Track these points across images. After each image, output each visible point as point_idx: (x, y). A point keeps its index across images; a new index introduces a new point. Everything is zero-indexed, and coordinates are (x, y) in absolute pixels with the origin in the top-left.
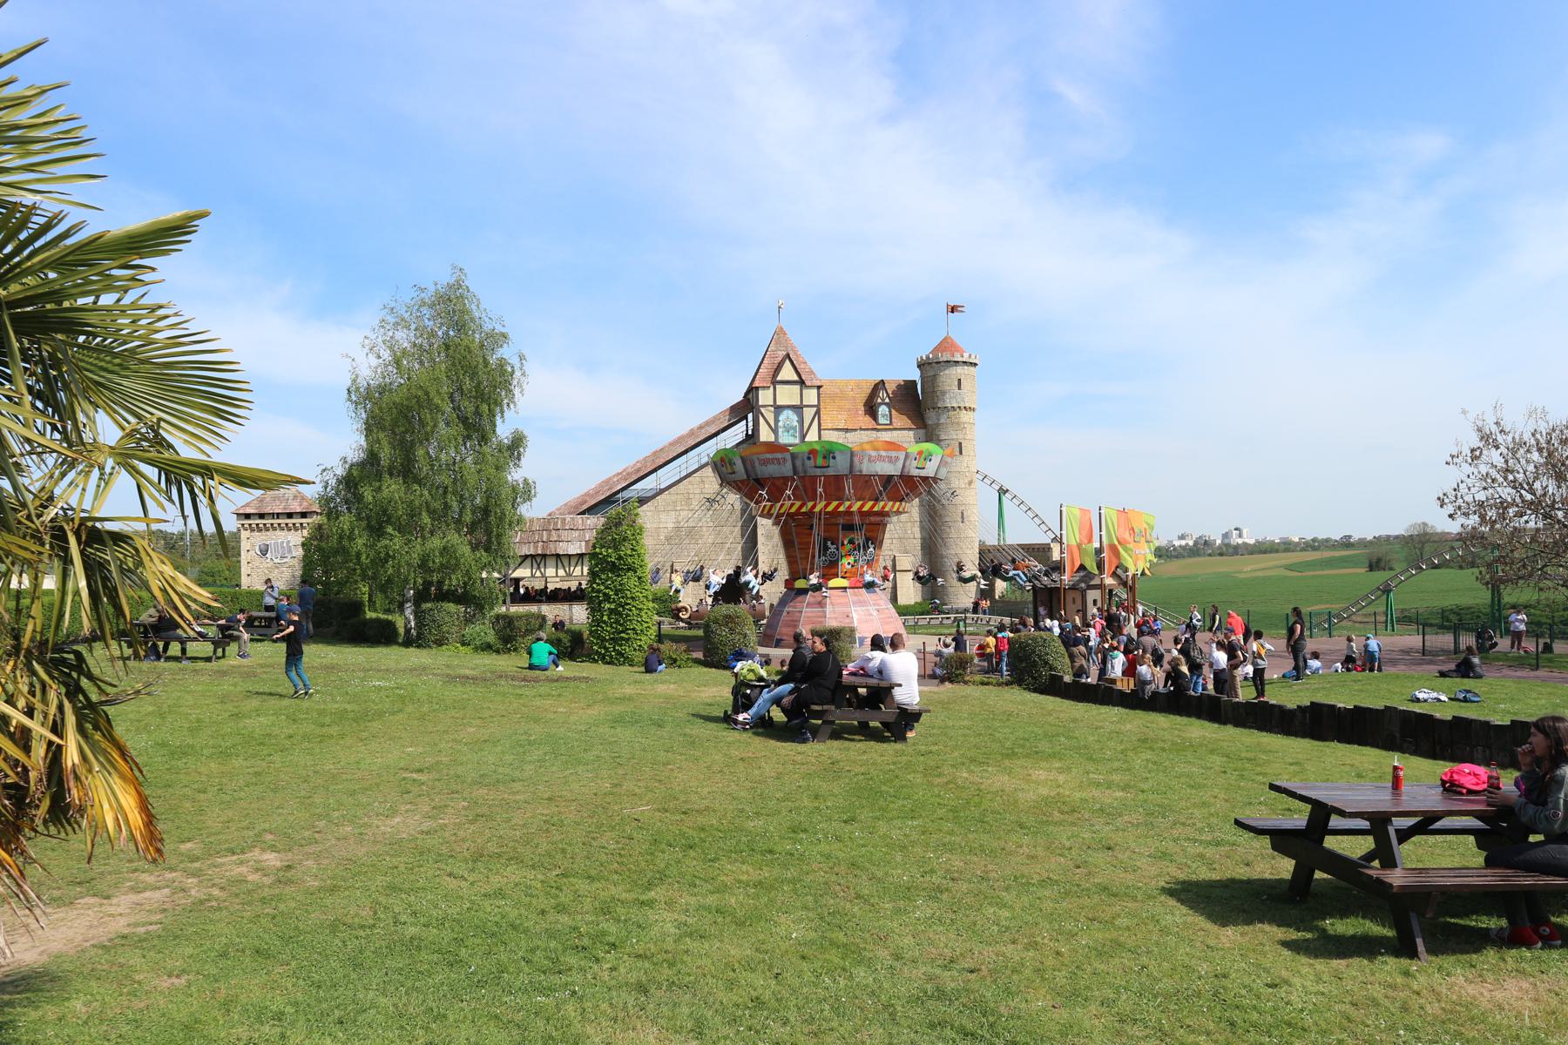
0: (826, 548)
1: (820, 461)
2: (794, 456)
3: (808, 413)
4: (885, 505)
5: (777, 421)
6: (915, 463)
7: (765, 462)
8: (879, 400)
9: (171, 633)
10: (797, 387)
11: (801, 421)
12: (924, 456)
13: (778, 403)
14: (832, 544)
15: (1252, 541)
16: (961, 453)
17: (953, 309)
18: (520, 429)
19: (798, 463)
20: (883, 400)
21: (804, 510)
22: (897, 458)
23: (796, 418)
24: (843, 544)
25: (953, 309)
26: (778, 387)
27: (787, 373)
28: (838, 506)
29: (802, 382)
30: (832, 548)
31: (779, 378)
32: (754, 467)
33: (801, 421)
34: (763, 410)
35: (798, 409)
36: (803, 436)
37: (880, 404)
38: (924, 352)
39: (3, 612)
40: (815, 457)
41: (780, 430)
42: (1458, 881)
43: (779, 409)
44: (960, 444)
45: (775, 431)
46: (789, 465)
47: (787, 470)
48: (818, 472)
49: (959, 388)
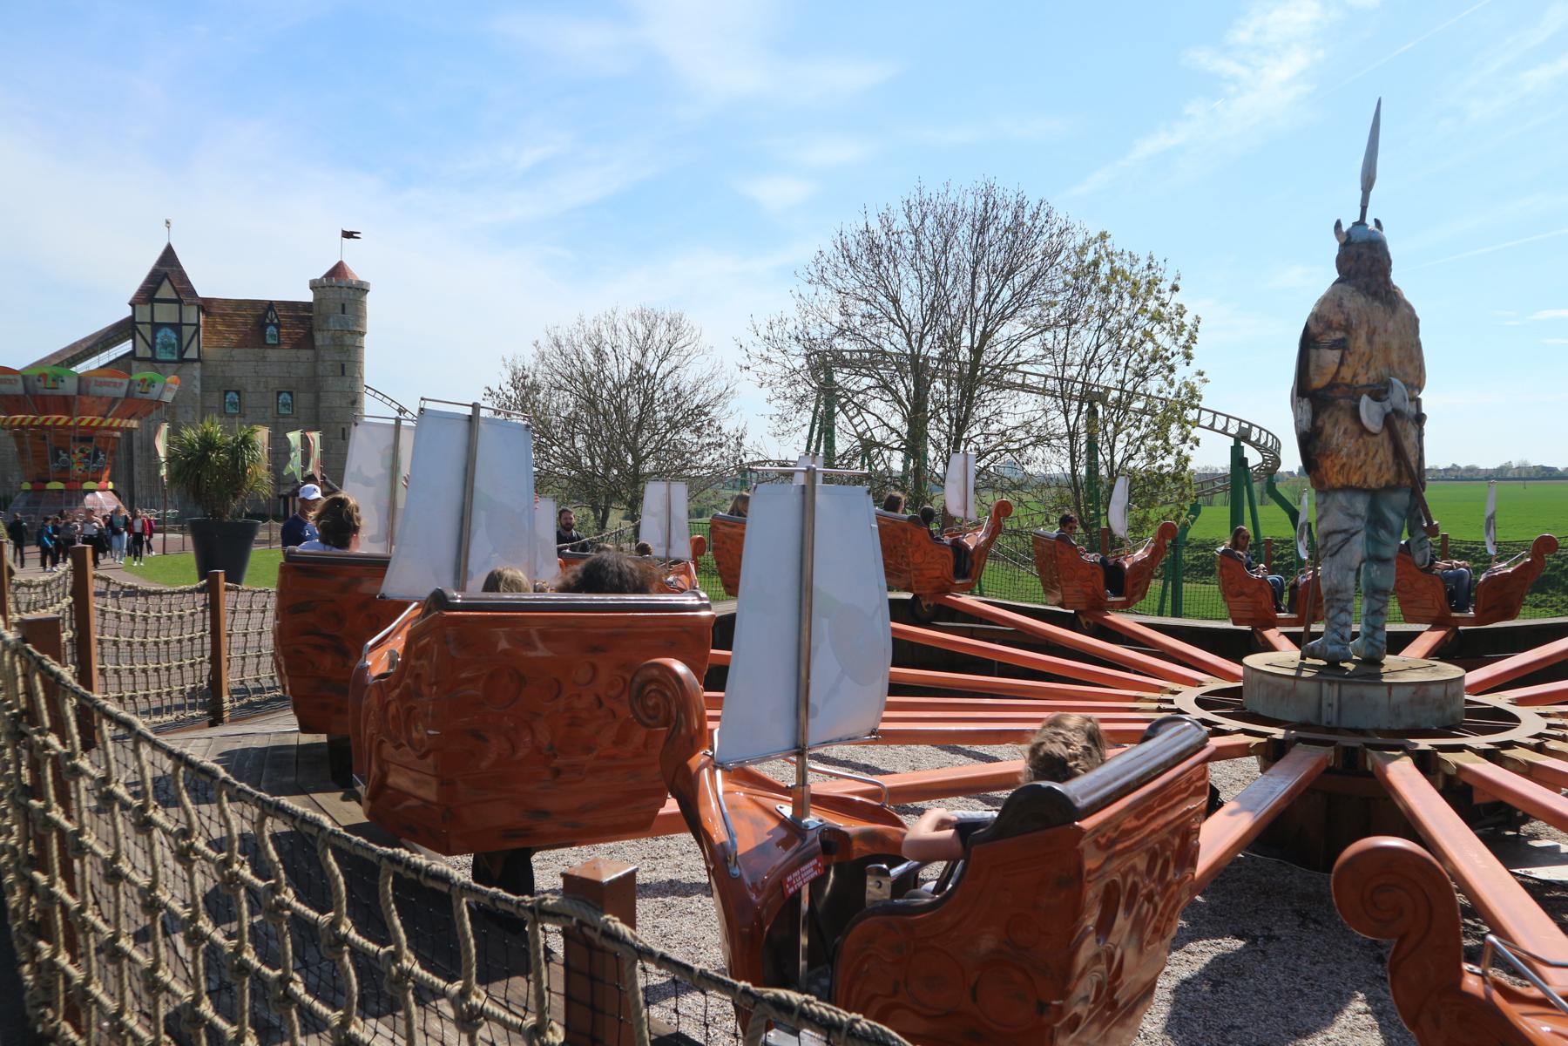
0: (59, 456)
1: (50, 383)
2: (25, 378)
3: (187, 332)
4: (92, 420)
5: (154, 338)
6: (138, 389)
7: (101, 384)
8: (268, 321)
9: (371, 700)
10: (176, 306)
11: (180, 339)
12: (146, 383)
13: (157, 320)
14: (64, 452)
15: (1427, 494)
16: (343, 374)
17: (348, 235)
18: (372, 289)
19: (132, 388)
20: (272, 321)
21: (71, 423)
22: (121, 384)
23: (174, 336)
24: (74, 453)
25: (348, 235)
26: (157, 306)
27: (166, 291)
28: (101, 422)
29: (179, 302)
30: (64, 456)
31: (195, 327)
32: (88, 386)
33: (180, 339)
34: (139, 326)
35: (177, 327)
36: (182, 352)
37: (268, 325)
38: (319, 273)
39: (1154, 1019)
40: (45, 381)
41: (158, 347)
42: (1266, 809)
43: (156, 327)
44: (343, 366)
45: (152, 347)
46: (124, 389)
47: (19, 389)
48: (48, 392)
49: (343, 312)
